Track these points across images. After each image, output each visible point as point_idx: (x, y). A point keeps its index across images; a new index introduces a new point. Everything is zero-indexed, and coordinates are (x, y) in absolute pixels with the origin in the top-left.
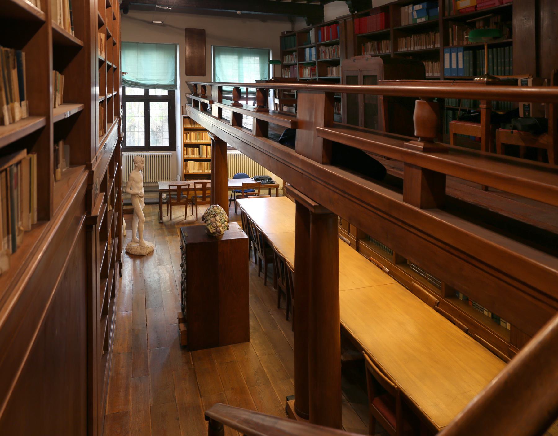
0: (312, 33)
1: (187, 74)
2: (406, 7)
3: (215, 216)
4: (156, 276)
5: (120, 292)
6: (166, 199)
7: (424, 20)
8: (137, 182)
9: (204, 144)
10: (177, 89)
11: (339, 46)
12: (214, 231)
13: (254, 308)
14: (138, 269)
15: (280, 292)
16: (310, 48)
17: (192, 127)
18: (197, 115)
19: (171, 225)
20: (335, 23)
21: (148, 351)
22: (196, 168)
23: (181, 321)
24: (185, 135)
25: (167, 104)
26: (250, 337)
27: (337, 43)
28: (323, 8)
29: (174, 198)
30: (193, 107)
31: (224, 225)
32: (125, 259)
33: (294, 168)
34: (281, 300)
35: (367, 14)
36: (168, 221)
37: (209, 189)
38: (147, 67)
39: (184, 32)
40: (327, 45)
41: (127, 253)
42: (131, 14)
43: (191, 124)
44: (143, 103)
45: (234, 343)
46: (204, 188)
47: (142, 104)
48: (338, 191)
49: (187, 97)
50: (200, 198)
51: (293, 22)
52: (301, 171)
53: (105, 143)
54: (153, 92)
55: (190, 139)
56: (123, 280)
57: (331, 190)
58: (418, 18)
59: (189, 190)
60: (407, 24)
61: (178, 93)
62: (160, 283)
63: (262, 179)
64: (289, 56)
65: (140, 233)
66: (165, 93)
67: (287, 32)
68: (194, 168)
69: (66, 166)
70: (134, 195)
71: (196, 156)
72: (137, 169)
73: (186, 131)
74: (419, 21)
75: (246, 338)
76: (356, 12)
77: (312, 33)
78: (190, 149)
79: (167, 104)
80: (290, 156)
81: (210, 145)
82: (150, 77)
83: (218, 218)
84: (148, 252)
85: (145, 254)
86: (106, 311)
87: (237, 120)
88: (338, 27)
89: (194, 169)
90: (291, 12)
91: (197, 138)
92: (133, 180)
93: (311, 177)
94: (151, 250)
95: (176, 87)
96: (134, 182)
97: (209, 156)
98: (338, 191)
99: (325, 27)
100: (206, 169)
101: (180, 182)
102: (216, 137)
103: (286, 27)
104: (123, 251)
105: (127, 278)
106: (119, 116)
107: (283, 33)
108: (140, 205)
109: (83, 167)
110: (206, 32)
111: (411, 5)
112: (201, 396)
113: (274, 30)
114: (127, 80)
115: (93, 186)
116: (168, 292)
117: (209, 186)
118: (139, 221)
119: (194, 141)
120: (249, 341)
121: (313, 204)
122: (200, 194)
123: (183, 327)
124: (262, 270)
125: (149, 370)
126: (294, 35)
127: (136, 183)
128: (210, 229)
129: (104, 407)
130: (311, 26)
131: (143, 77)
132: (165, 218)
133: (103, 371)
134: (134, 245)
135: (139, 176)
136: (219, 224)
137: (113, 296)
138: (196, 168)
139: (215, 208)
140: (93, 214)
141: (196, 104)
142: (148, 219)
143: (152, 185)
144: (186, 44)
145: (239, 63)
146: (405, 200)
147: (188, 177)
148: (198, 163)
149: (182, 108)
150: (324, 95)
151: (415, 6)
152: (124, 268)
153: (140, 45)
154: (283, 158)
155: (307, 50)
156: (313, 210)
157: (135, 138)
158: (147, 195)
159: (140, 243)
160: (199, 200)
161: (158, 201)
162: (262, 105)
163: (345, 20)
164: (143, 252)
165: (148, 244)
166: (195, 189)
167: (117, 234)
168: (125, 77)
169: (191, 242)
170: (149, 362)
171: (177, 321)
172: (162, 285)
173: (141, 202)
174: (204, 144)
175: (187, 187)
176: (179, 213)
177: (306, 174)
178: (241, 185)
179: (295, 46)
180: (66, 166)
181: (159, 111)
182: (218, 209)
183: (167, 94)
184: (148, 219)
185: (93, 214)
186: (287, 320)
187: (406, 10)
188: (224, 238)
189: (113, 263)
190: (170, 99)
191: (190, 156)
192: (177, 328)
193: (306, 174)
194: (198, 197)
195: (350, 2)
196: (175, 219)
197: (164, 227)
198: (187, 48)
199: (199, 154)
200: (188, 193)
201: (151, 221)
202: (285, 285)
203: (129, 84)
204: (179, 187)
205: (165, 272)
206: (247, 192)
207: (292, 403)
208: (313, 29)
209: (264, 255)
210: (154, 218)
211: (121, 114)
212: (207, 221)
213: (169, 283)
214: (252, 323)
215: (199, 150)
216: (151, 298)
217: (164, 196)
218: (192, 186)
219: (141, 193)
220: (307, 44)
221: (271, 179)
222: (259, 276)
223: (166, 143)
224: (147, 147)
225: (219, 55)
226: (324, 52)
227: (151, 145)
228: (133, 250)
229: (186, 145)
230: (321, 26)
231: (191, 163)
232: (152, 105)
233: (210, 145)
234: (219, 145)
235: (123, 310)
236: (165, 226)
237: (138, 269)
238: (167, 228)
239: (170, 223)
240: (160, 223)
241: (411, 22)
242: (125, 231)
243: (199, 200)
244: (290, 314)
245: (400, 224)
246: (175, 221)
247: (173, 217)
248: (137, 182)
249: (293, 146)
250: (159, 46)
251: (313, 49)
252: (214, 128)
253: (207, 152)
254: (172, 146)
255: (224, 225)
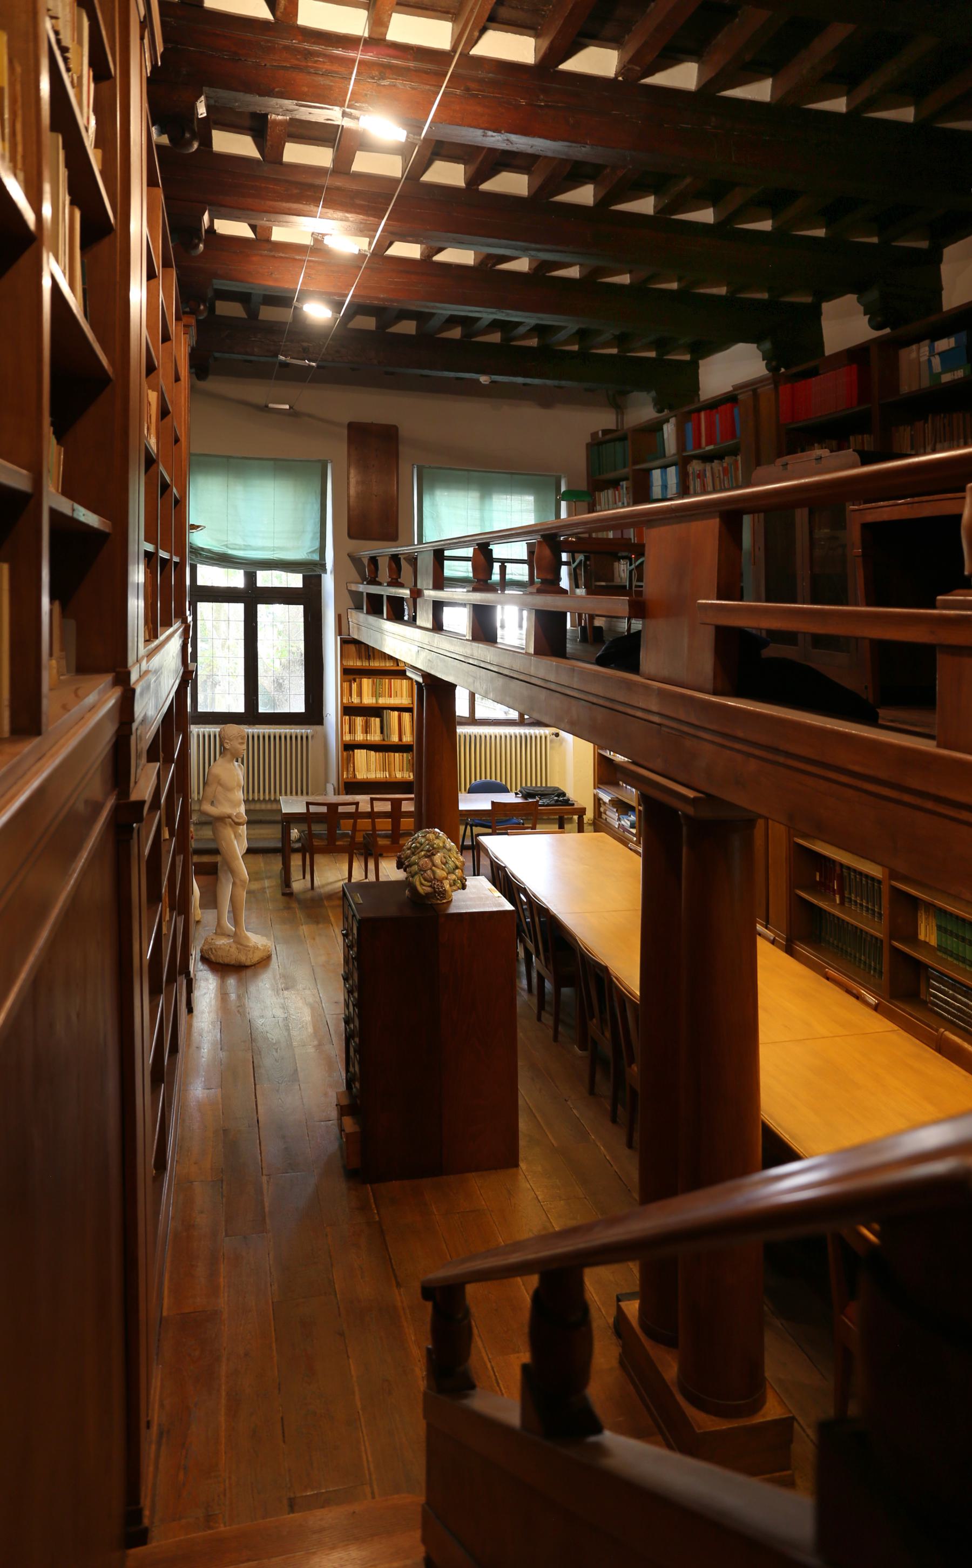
0: (669, 430)
1: (351, 536)
2: (914, 347)
3: (430, 854)
4: (279, 1013)
5: (189, 1045)
6: (298, 840)
7: (960, 374)
8: (229, 789)
9: (394, 709)
10: (325, 571)
11: (739, 458)
12: (429, 890)
13: (528, 1093)
14: (233, 996)
15: (596, 1060)
16: (664, 467)
17: (365, 662)
18: (381, 631)
19: (313, 900)
20: (730, 399)
21: (265, 1179)
22: (373, 767)
23: (343, 1110)
24: (346, 685)
25: (301, 607)
26: (521, 1156)
27: (734, 452)
28: (698, 367)
29: (319, 836)
30: (368, 613)
31: (453, 877)
32: (199, 974)
33: (639, 714)
34: (598, 1076)
35: (813, 372)
36: (305, 892)
37: (408, 814)
38: (250, 518)
39: (345, 432)
40: (707, 458)
41: (205, 959)
42: (212, 384)
43: (360, 658)
44: (241, 607)
45: (477, 1169)
46: (396, 813)
47: (237, 610)
48: (757, 752)
49: (351, 592)
50: (386, 836)
51: (618, 406)
52: (656, 719)
53: (156, 670)
54: (265, 579)
55: (360, 694)
56: (195, 1020)
57: (739, 751)
58: (944, 371)
59: (356, 815)
60: (915, 388)
61: (328, 582)
62: (288, 1030)
63: (543, 795)
64: (610, 492)
65: (237, 914)
66: (295, 581)
67: (605, 432)
68: (367, 767)
69: (68, 671)
70: (222, 819)
71: (375, 737)
72: (229, 756)
73: (349, 674)
74: (946, 378)
75: (509, 1159)
76: (783, 370)
77: (669, 430)
78: (359, 721)
79: (301, 607)
80: (630, 685)
81: (409, 710)
82: (259, 542)
83: (438, 858)
84: (256, 957)
85: (248, 963)
86: (161, 1074)
87: (483, 629)
88: (736, 411)
89: (368, 770)
90: (613, 380)
91: (376, 694)
92: (220, 783)
93: (685, 728)
94: (265, 954)
95: (323, 566)
96: (220, 788)
97: (408, 738)
98: (757, 752)
99: (703, 415)
100: (401, 769)
101: (332, 798)
102: (427, 676)
103: (604, 420)
104: (195, 954)
105: (206, 1015)
106: (184, 620)
107: (594, 435)
108: (237, 843)
109: (109, 678)
110: (403, 432)
111: (927, 342)
112: (398, 1285)
113: (574, 426)
114: (202, 549)
115: (133, 738)
116: (310, 1050)
117: (408, 807)
118: (234, 884)
119: (368, 700)
120: (517, 1165)
121: (691, 794)
122: (385, 825)
123: (350, 1124)
124: (547, 1008)
125: (268, 1221)
126: (623, 438)
127: (227, 789)
128: (418, 884)
129: (161, 1298)
130: (666, 411)
131: (239, 541)
132: (298, 885)
133: (157, 1213)
134: (222, 942)
135: (234, 773)
136: (440, 873)
137: (174, 1049)
138: (373, 767)
139: (431, 836)
140: (134, 797)
141: (374, 606)
142: (255, 886)
143: (263, 807)
144: (349, 466)
145: (482, 510)
146: (938, 746)
147: (353, 787)
148: (379, 755)
149: (339, 619)
150: (717, 520)
151: (936, 343)
152: (197, 994)
153: (236, 464)
154: (610, 695)
155: (656, 474)
156: (690, 811)
157: (221, 692)
158: (252, 832)
159: (237, 937)
160: (381, 842)
161: (280, 845)
162: (549, 577)
163: (755, 391)
164: (243, 959)
165: (257, 940)
166: (372, 815)
167: (182, 905)
168: (198, 539)
169: (371, 915)
170: (267, 1204)
171: (334, 1114)
172: (294, 1033)
173: (237, 836)
174: (394, 709)
175: (352, 809)
176: (332, 874)
177: (674, 725)
178: (488, 807)
179: (625, 467)
180: (68, 671)
181: (281, 626)
182: (438, 837)
183: (300, 585)
184: (255, 886)
185: (134, 797)
186: (614, 1120)
187: (914, 355)
188: (453, 909)
189: (171, 976)
190: (308, 598)
191: (360, 737)
192: (336, 1130)
193: (674, 725)
194: (380, 836)
195: (767, 345)
196: (323, 886)
197: (295, 905)
198: (352, 472)
199: (382, 732)
200: (355, 825)
201: (263, 890)
202: (608, 1034)
203: (207, 557)
204: (333, 807)
205: (300, 1004)
206: (502, 820)
207: (632, 1308)
208: (673, 420)
209: (551, 967)
210: (270, 885)
211: (190, 619)
212: (410, 866)
213: (310, 1030)
214: (523, 1125)
215: (382, 722)
216: (267, 1061)
217: (295, 833)
218: (365, 807)
219: (238, 815)
220: (656, 459)
221: (564, 794)
222: (539, 1019)
223: (298, 706)
224: (251, 715)
225: (432, 488)
226: (699, 476)
227: (260, 711)
228: (220, 953)
229: (349, 711)
230: (690, 412)
231: (360, 754)
232: (264, 611)
233: (409, 710)
234: (436, 693)
235: (197, 1090)
236: (299, 901)
237: (233, 996)
238: (306, 908)
239: (309, 895)
240: (284, 894)
241: (926, 383)
242: (199, 911)
243: (381, 842)
244: (620, 1109)
245: (929, 805)
246: (322, 891)
247: (317, 882)
248: (229, 789)
249: (634, 667)
250: (282, 466)
251: (672, 471)
252: (424, 654)
253: (403, 729)
254: (314, 711)
255: (453, 877)
